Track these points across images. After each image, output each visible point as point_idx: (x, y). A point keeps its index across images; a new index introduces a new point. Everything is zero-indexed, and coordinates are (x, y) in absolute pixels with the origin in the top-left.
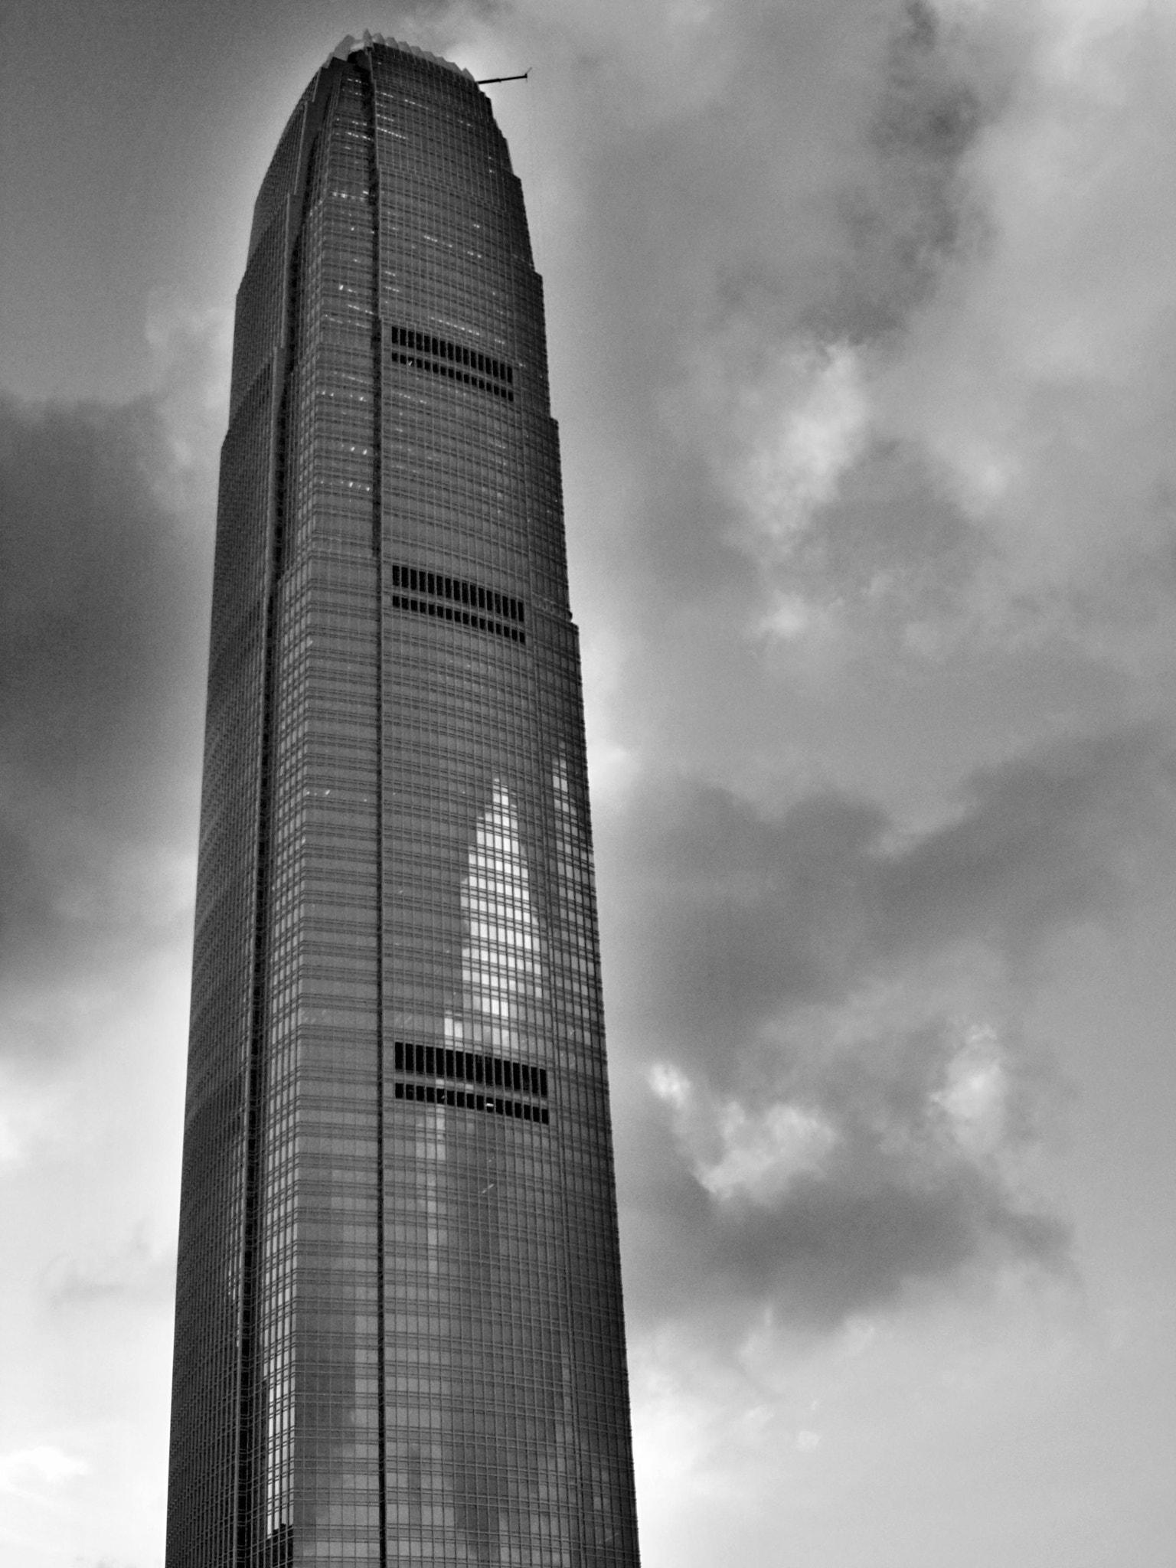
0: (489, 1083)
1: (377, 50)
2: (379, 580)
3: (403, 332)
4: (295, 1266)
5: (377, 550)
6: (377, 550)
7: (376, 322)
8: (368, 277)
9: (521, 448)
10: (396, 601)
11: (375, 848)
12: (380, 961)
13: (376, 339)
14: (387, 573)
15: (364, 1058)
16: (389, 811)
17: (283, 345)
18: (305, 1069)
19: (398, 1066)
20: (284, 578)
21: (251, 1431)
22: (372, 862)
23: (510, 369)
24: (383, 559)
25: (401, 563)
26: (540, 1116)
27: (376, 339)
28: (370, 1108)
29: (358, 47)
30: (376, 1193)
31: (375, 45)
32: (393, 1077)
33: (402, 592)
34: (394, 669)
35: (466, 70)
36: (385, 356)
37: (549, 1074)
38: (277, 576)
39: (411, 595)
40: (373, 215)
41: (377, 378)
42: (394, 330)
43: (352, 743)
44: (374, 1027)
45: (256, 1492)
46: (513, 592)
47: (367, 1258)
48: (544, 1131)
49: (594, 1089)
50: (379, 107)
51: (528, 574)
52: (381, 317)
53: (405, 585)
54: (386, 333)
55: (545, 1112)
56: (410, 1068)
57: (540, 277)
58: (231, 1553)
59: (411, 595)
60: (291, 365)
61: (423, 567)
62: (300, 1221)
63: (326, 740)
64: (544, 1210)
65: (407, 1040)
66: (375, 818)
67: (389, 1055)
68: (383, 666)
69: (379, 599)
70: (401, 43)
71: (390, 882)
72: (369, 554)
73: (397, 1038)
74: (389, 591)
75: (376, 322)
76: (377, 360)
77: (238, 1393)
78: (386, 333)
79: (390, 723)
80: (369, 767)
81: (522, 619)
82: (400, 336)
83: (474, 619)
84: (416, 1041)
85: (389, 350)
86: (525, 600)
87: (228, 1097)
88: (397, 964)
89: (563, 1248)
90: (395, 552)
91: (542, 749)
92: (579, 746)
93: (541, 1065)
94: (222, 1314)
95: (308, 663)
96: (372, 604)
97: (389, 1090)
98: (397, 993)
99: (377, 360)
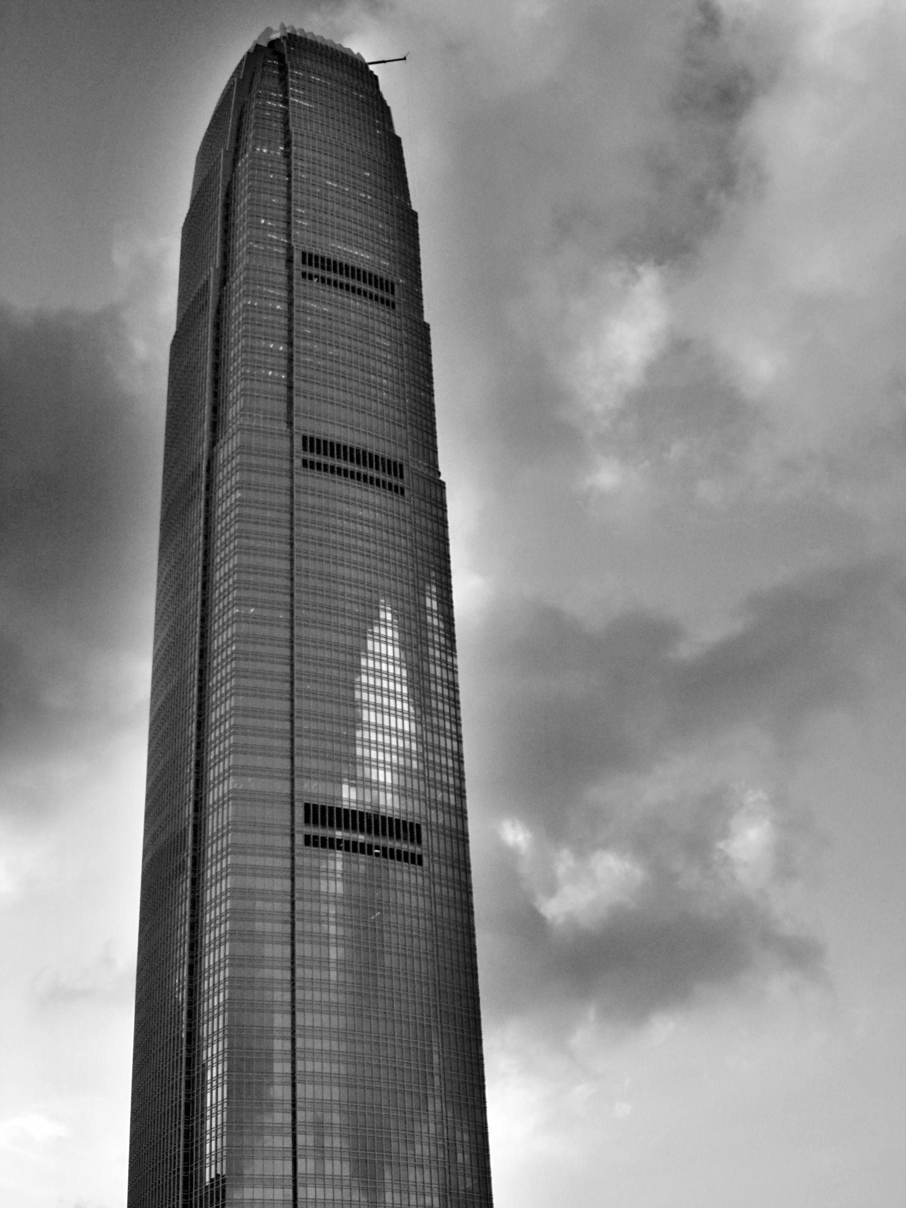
1: (290, 38)
2: (292, 446)
4: (227, 975)
5: (290, 423)
6: (290, 423)
7: (289, 248)
10: (305, 463)
13: (290, 261)
14: (298, 442)
15: (281, 815)
17: (218, 265)
18: (235, 823)
19: (307, 821)
20: (218, 445)
21: (193, 1103)
23: (393, 285)
25: (309, 434)
26: (416, 860)
27: (290, 261)
28: (285, 853)
29: (276, 36)
31: (289, 34)
36: (297, 274)
37: (423, 827)
38: (213, 443)
39: (316, 458)
42: (304, 254)
43: (272, 572)
45: (197, 1149)
46: (395, 456)
48: (419, 871)
50: (292, 82)
52: (294, 244)
54: (297, 257)
55: (420, 857)
56: (315, 823)
59: (316, 458)
60: (224, 281)
61: (326, 437)
62: (231, 940)
65: (313, 801)
68: (295, 513)
70: (309, 33)
72: (284, 426)
74: (300, 455)
75: (289, 248)
76: (290, 277)
78: (297, 257)
79: (300, 556)
82: (307, 258)
84: (320, 802)
85: (299, 270)
86: (404, 463)
90: (305, 425)
91: (423, 678)
93: (417, 820)
95: (237, 511)
96: (286, 465)
97: (299, 840)
99: (290, 277)
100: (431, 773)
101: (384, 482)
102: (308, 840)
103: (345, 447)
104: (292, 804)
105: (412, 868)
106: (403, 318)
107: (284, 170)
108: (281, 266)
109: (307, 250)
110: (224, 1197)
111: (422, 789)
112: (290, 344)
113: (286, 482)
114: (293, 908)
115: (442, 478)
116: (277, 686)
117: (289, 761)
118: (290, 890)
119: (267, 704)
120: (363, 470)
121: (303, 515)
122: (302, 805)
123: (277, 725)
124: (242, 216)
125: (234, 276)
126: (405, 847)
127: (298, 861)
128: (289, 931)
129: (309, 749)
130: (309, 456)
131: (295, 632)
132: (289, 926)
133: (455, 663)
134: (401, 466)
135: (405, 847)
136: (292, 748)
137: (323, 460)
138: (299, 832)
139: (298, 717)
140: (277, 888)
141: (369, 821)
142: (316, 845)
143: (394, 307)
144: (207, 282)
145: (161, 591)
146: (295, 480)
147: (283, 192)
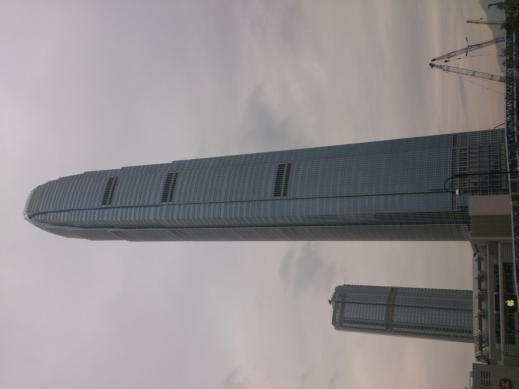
0: (282, 176)
1: (29, 212)
5: (158, 206)
6: (158, 206)
7: (100, 209)
9: (134, 175)
10: (109, 204)
11: (234, 203)
12: (255, 201)
13: (104, 208)
14: (164, 203)
17: (107, 229)
19: (280, 196)
20: (165, 226)
25: (161, 200)
26: (289, 166)
27: (104, 208)
29: (27, 216)
30: (289, 200)
31: (27, 212)
32: (282, 196)
33: (168, 200)
35: (31, 192)
36: (110, 206)
37: (280, 164)
38: (165, 227)
41: (115, 208)
43: (99, 214)
44: (270, 201)
45: (313, 223)
47: (87, 210)
49: (167, 166)
50: (35, 212)
51: (162, 173)
53: (166, 199)
55: (288, 164)
56: (280, 193)
58: (429, 226)
63: (236, 213)
64: (324, 163)
65: (273, 194)
67: (277, 198)
70: (25, 207)
72: (159, 208)
76: (110, 208)
77: (360, 226)
79: (155, 203)
80: (114, 210)
81: (173, 174)
82: (104, 203)
87: (174, 232)
88: (250, 197)
92: (242, 156)
97: (285, 197)
99: (110, 208)
102: (285, 195)
103: (105, 192)
104: (274, 200)
108: (106, 211)
113: (182, 206)
114: (374, 195)
118: (319, 199)
120: (112, 187)
121: (217, 199)
122: (102, 206)
125: (110, 224)
128: (312, 199)
129: (188, 200)
130: (168, 200)
131: (182, 203)
132: (330, 198)
134: (169, 174)
136: (293, 199)
139: (242, 200)
140: (98, 212)
141: (278, 179)
144: (112, 232)
146: (207, 202)
147: (82, 211)
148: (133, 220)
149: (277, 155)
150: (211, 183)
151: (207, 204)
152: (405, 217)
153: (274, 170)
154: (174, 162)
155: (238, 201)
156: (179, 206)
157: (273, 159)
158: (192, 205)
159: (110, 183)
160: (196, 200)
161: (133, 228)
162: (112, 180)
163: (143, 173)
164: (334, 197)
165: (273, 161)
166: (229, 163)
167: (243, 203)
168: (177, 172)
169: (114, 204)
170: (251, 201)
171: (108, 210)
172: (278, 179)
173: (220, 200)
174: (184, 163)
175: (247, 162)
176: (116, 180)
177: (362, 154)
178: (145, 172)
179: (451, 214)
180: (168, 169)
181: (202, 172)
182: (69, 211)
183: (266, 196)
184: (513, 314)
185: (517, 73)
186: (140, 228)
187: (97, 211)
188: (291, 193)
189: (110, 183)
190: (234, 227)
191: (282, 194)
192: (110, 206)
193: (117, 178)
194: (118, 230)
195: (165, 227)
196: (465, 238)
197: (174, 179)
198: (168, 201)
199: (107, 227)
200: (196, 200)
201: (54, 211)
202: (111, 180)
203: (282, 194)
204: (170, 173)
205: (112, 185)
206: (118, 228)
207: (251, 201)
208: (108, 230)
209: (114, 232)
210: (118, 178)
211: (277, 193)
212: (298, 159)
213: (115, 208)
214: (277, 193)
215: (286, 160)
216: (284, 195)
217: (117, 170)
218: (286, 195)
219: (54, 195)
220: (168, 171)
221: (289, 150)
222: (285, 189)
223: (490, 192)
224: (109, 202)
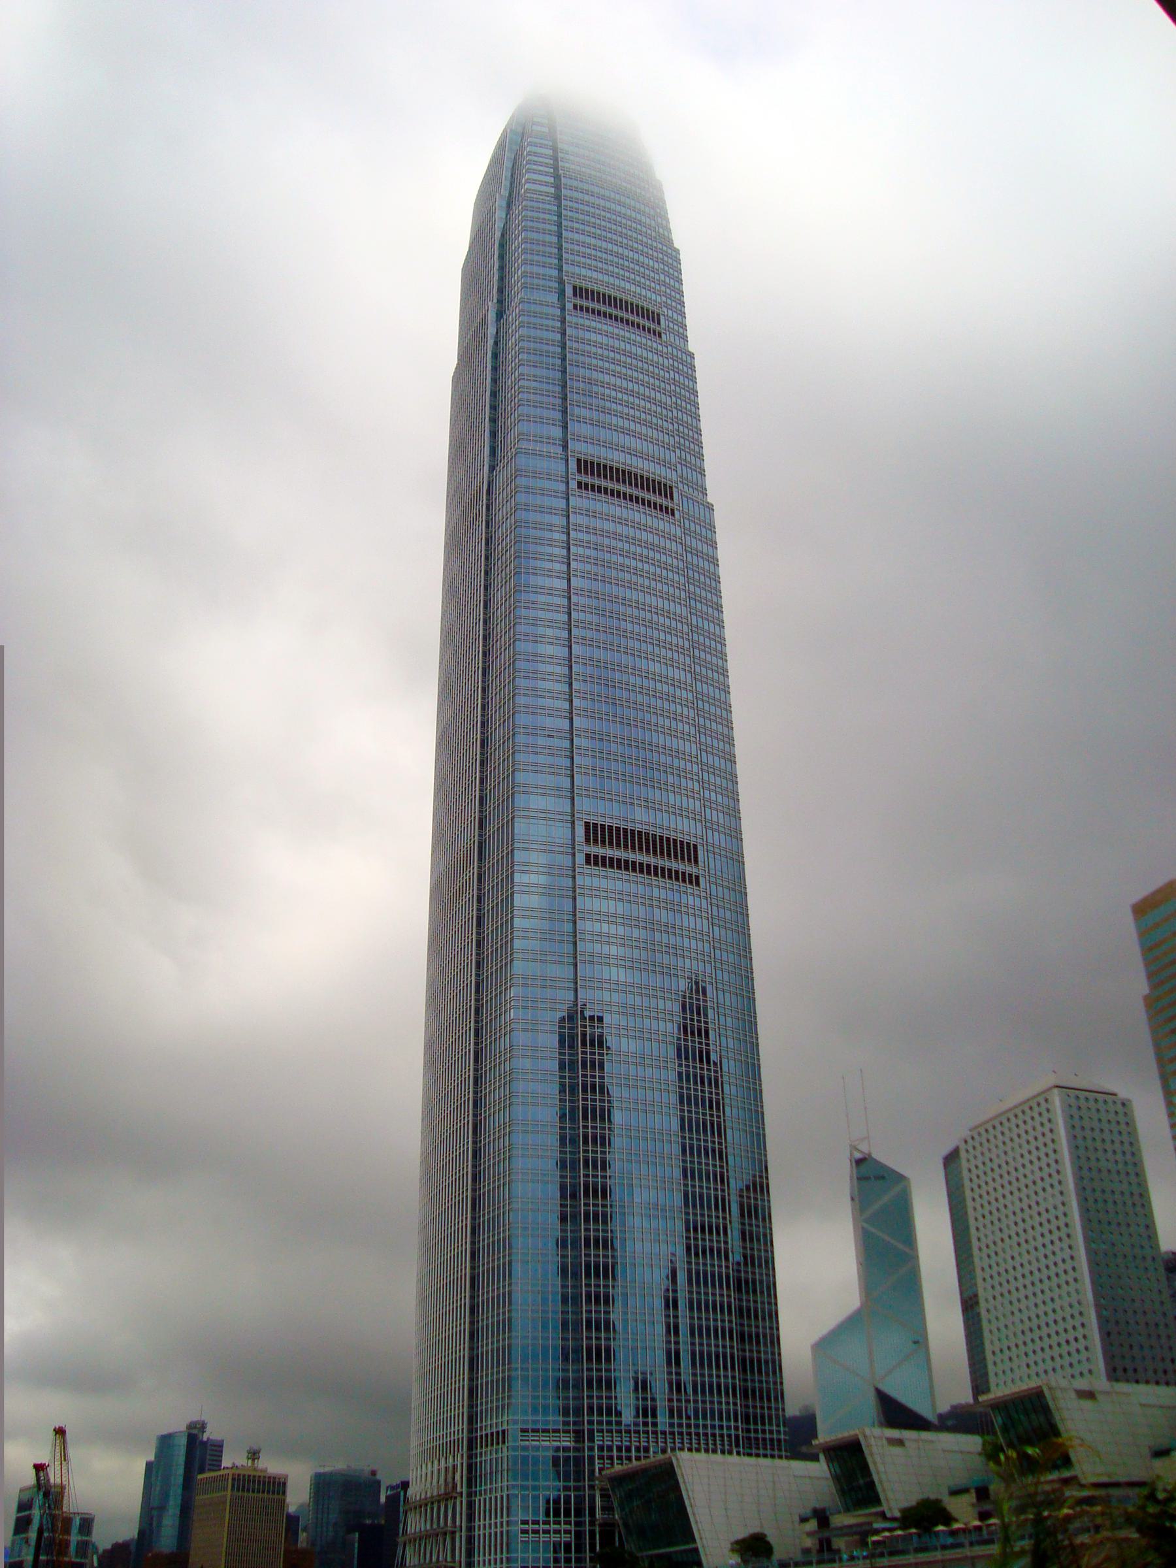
3: (581, 289)
5: (565, 447)
6: (565, 447)
8: (559, 362)
10: (579, 484)
13: (562, 293)
14: (573, 465)
15: (561, 833)
16: (581, 795)
17: (495, 301)
19: (587, 840)
22: (564, 629)
23: (658, 315)
24: (569, 453)
25: (583, 457)
26: (695, 880)
27: (562, 293)
28: (566, 818)
34: (588, 926)
36: (569, 306)
37: (699, 848)
38: (492, 468)
39: (585, 303)
40: (558, 237)
42: (575, 288)
43: (549, 511)
46: (665, 478)
48: (696, 892)
54: (569, 291)
55: (697, 878)
57: (679, 250)
59: (585, 303)
60: (500, 315)
61: (599, 460)
65: (592, 820)
66: (572, 967)
69: (567, 483)
71: (584, 940)
72: (559, 450)
73: (586, 818)
74: (575, 478)
75: (561, 282)
78: (569, 291)
81: (672, 498)
82: (578, 291)
83: (627, 321)
84: (600, 821)
85: (571, 302)
87: (475, 500)
89: (686, 606)
91: (694, 662)
93: (693, 841)
94: (466, 1046)
96: (562, 487)
97: (580, 859)
98: (588, 906)
99: (563, 309)
100: (707, 792)
101: (670, 871)
104: (573, 823)
105: (690, 889)
106: (674, 410)
107: (559, 380)
108: (554, 298)
109: (578, 284)
110: (510, 1304)
111: (694, 752)
112: (565, 427)
113: (562, 504)
115: (710, 499)
116: (557, 566)
117: (569, 779)
119: (547, 501)
123: (557, 600)
124: (516, 288)
126: (681, 867)
127: (579, 880)
133: (732, 752)
134: (671, 488)
135: (681, 867)
137: (596, 481)
138: (580, 819)
141: (647, 840)
142: (596, 864)
143: (660, 336)
145: (454, 425)
148: (517, 483)
149: (695, 477)
150: (637, 602)
151: (566, 705)
152: (494, 1221)
153: (682, 828)
154: (710, 508)
155: (572, 701)
156: (561, 512)
157: (719, 881)
158: (565, 538)
159: (643, 313)
160: (580, 536)
161: (496, 387)
162: (666, 496)
163: (675, 411)
164: (576, 957)
165: (718, 965)
166: (715, 827)
167: (565, 717)
168: (676, 512)
169: (574, 320)
170: (568, 522)
171: (556, 302)
172: (647, 840)
173: (584, 962)
174: (695, 465)
175: (721, 911)
176: (667, 508)
177: (718, 971)
178: (677, 418)
179: (491, 1489)
180: (686, 487)
181: (686, 727)
182: (558, 197)
183: (592, 963)
184: (66, 1537)
185: (994, 1528)
186: (495, 369)
187: (555, 273)
188: (593, 879)
189: (643, 313)
190: (484, 690)
191: (594, 850)
192: (569, 306)
193: (673, 511)
194: (492, 330)
195: (502, 317)
196: (436, 1462)
197: (677, 872)
198: (580, 478)
199: (500, 301)
200: (580, 536)
201: (561, 223)
202: (666, 491)
203: (594, 850)
204: (674, 490)
205: (647, 496)
206: (497, 333)
207: (568, 522)
208: (490, 303)
209: (484, 322)
210: (673, 514)
211: (595, 833)
212: (715, 913)
213: (563, 321)
214: (595, 833)
215: (712, 872)
216: (588, 856)
217: (685, 338)
218: (588, 862)
219: (622, 346)
220: (680, 485)
221: (763, 1078)
222: (611, 859)
223: (576, 1488)
224: (586, 485)
